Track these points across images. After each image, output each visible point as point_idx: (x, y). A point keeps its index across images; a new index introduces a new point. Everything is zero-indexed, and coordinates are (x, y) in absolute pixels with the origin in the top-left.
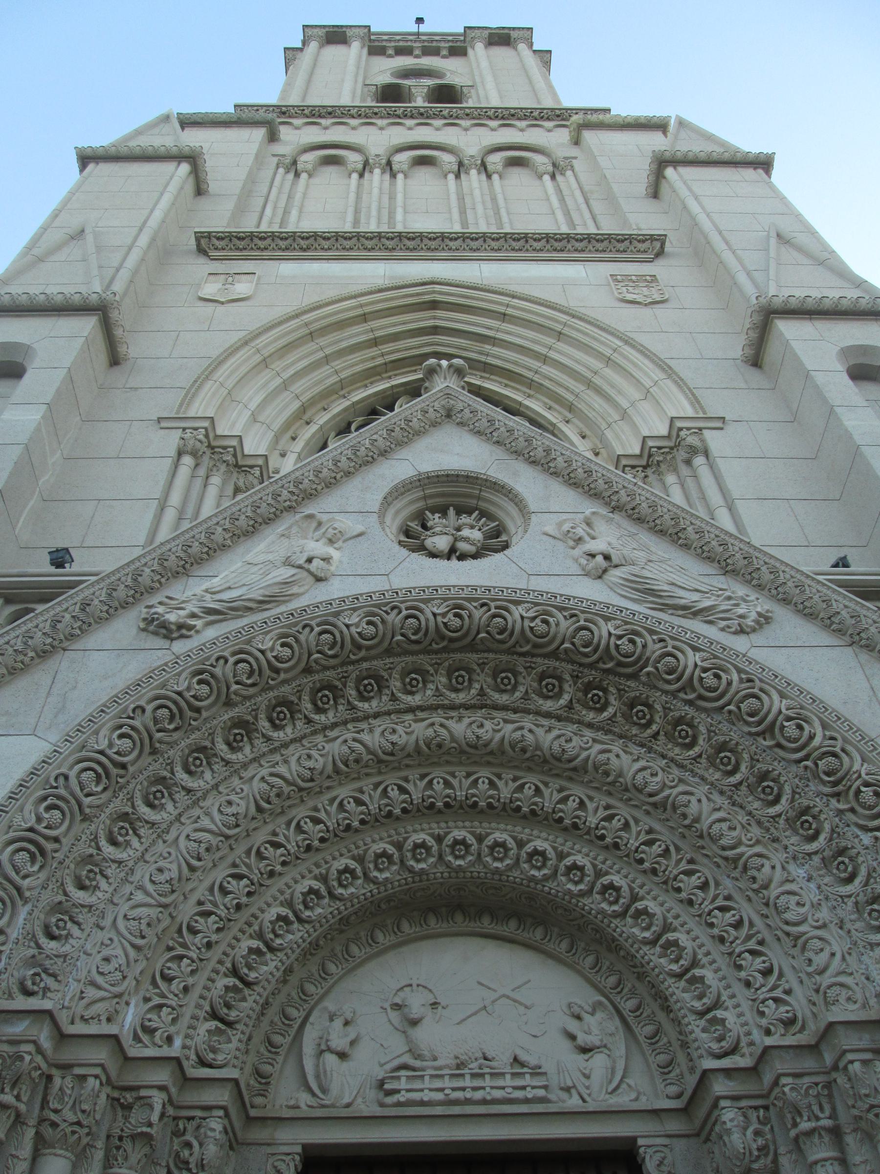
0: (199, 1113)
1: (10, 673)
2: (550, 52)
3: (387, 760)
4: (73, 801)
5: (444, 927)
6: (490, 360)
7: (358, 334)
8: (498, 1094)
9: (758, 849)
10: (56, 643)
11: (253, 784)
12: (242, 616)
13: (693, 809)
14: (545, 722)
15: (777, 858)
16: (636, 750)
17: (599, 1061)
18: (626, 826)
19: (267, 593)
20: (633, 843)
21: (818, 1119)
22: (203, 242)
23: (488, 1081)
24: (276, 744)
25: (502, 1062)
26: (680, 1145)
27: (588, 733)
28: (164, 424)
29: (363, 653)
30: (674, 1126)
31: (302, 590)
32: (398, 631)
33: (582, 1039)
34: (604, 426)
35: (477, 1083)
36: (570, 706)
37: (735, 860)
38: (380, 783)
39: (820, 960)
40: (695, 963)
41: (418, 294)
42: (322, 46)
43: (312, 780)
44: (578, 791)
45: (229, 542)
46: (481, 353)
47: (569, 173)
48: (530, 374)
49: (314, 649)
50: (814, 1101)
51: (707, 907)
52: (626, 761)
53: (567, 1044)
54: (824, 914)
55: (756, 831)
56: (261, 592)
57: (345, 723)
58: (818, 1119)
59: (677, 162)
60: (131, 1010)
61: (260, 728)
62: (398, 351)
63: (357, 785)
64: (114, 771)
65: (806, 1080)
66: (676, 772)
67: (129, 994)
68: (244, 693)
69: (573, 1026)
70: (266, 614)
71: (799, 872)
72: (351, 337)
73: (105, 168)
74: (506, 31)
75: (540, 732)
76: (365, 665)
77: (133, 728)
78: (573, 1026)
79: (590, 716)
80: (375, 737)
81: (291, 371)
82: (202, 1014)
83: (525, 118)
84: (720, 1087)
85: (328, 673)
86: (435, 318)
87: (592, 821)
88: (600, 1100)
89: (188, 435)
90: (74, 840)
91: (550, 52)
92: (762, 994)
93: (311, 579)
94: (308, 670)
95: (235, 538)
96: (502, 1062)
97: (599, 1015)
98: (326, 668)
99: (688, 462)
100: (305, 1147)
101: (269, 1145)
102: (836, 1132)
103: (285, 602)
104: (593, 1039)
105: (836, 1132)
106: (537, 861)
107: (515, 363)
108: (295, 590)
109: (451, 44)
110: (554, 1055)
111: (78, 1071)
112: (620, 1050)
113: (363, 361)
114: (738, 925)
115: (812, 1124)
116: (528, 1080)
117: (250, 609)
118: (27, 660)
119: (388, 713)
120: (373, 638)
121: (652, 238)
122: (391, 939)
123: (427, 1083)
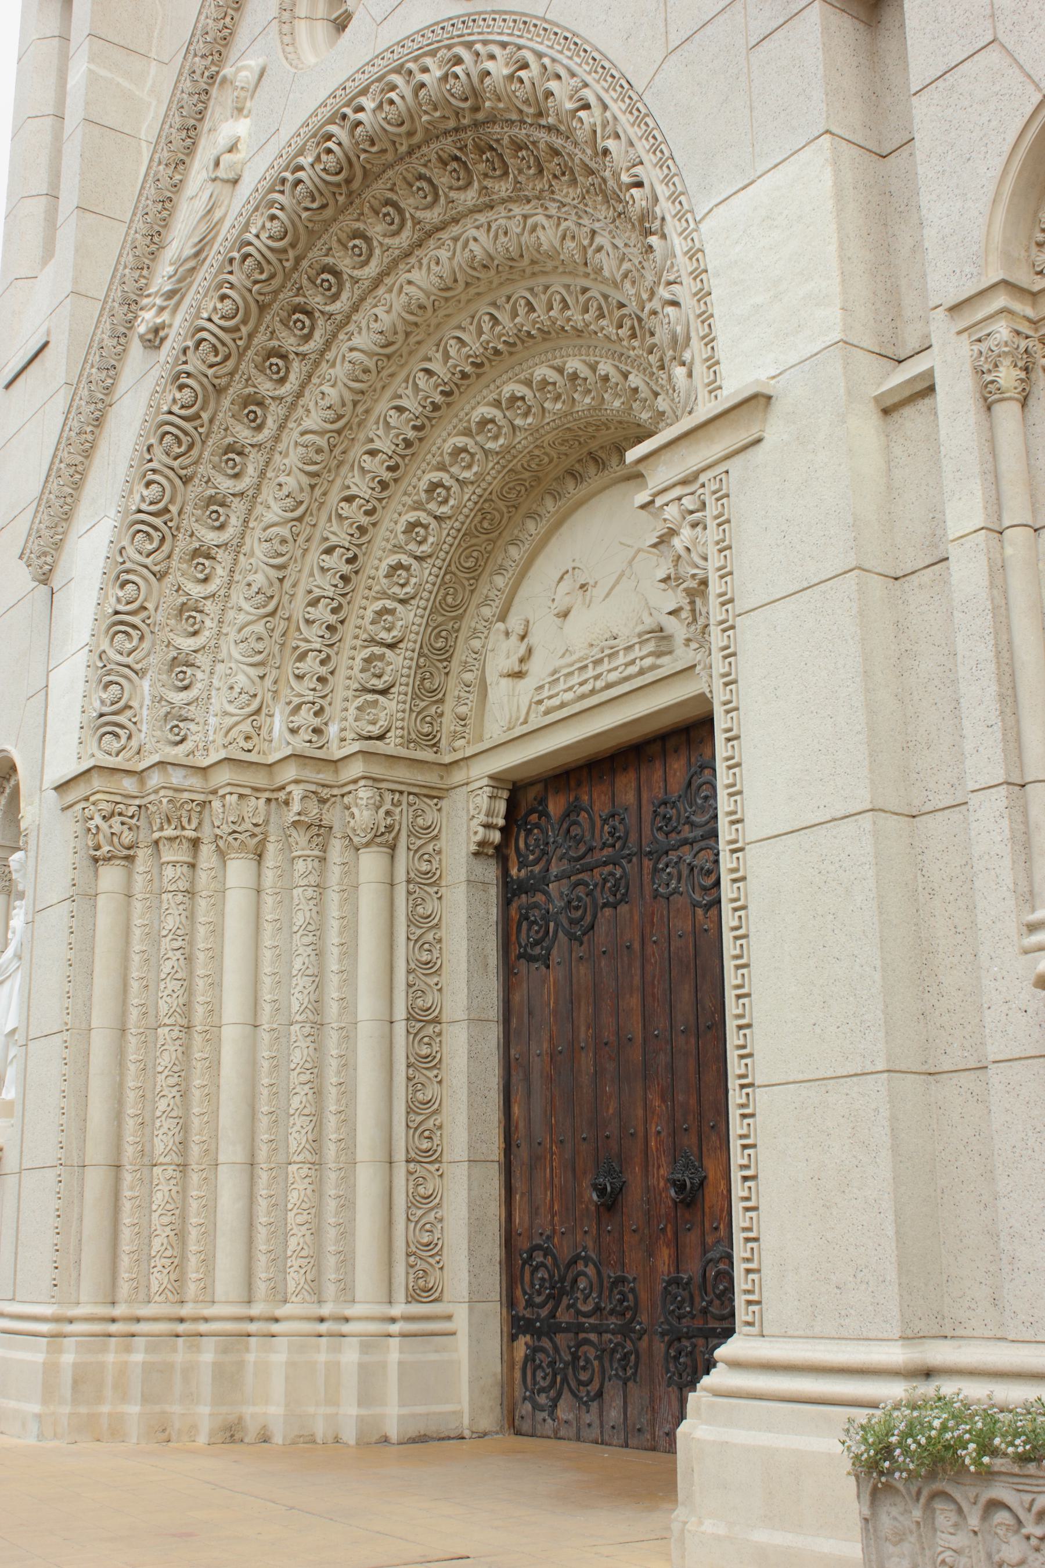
0: (351, 787)
1: (87, 457)
3: (391, 353)
4: (139, 568)
5: (584, 489)
10: (100, 406)
11: (291, 458)
12: (192, 283)
19: (197, 240)
21: (183, 828)
24: (289, 399)
29: (291, 254)
31: (223, 209)
32: (299, 210)
38: (408, 376)
43: (340, 417)
45: (179, 177)
49: (249, 284)
50: (185, 814)
56: (190, 243)
57: (335, 336)
58: (183, 828)
60: (277, 719)
61: (265, 393)
63: (389, 393)
64: (158, 521)
65: (186, 796)
67: (268, 706)
68: (225, 370)
70: (207, 262)
76: (305, 263)
77: (154, 471)
80: (363, 338)
82: (350, 694)
85: (281, 296)
90: (162, 600)
93: (228, 187)
94: (262, 308)
95: (181, 167)
98: (276, 292)
100: (491, 777)
101: (467, 784)
103: (214, 238)
108: (218, 214)
111: (221, 792)
115: (177, 833)
117: (194, 269)
118: (90, 437)
119: (362, 299)
120: (286, 233)
122: (543, 526)
123: (621, 659)
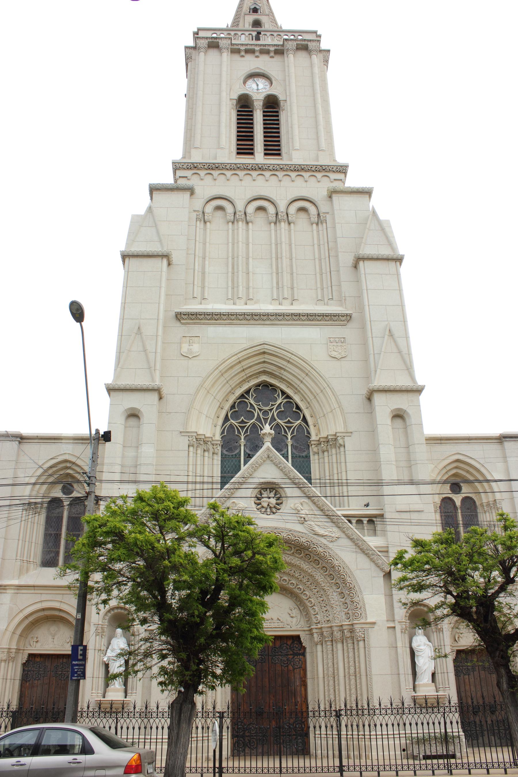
2: (329, 51)
6: (283, 377)
7: (238, 368)
8: (274, 626)
9: (328, 588)
13: (317, 578)
14: (288, 556)
15: (331, 590)
16: (307, 563)
17: (294, 620)
18: (303, 577)
20: (304, 581)
22: (178, 316)
23: (272, 624)
25: (275, 618)
26: (308, 636)
27: (297, 559)
28: (183, 434)
30: (307, 633)
33: (292, 615)
34: (318, 417)
35: (270, 624)
36: (293, 553)
37: (324, 589)
39: (335, 612)
40: (314, 605)
41: (259, 350)
42: (205, 53)
44: (294, 569)
46: (280, 373)
47: (324, 224)
48: (296, 386)
51: (317, 596)
52: (305, 566)
53: (289, 615)
54: (337, 603)
55: (328, 584)
59: (364, 259)
62: (251, 372)
66: (314, 569)
69: (290, 612)
71: (335, 594)
72: (236, 371)
73: (133, 261)
74: (306, 43)
75: (286, 558)
78: (290, 612)
79: (297, 556)
81: (216, 392)
83: (308, 170)
84: (314, 631)
86: (264, 358)
87: (296, 575)
88: (293, 628)
89: (190, 439)
91: (329, 51)
92: (325, 614)
96: (275, 618)
97: (296, 610)
99: (339, 448)
102: (332, 641)
104: (293, 615)
105: (332, 641)
106: (285, 581)
107: (292, 380)
109: (276, 48)
110: (285, 618)
112: (299, 617)
113: (239, 379)
114: (323, 601)
116: (280, 624)
121: (347, 315)
